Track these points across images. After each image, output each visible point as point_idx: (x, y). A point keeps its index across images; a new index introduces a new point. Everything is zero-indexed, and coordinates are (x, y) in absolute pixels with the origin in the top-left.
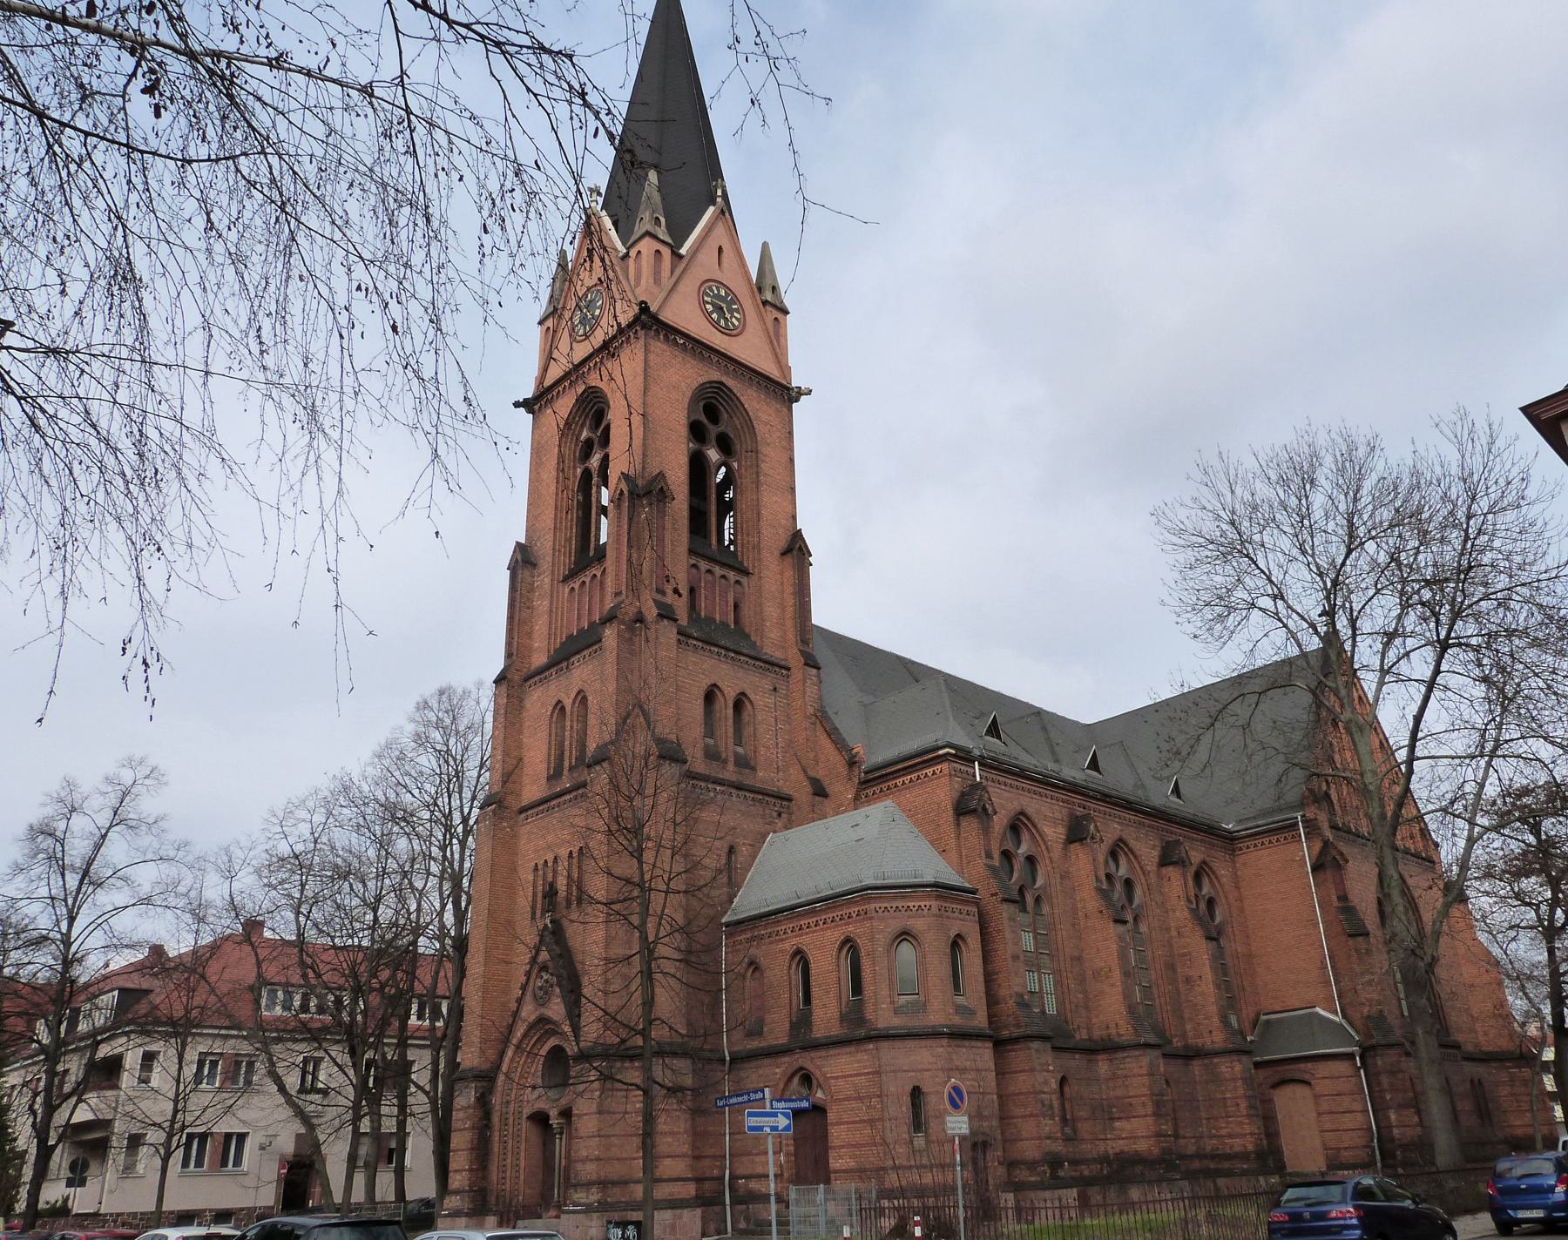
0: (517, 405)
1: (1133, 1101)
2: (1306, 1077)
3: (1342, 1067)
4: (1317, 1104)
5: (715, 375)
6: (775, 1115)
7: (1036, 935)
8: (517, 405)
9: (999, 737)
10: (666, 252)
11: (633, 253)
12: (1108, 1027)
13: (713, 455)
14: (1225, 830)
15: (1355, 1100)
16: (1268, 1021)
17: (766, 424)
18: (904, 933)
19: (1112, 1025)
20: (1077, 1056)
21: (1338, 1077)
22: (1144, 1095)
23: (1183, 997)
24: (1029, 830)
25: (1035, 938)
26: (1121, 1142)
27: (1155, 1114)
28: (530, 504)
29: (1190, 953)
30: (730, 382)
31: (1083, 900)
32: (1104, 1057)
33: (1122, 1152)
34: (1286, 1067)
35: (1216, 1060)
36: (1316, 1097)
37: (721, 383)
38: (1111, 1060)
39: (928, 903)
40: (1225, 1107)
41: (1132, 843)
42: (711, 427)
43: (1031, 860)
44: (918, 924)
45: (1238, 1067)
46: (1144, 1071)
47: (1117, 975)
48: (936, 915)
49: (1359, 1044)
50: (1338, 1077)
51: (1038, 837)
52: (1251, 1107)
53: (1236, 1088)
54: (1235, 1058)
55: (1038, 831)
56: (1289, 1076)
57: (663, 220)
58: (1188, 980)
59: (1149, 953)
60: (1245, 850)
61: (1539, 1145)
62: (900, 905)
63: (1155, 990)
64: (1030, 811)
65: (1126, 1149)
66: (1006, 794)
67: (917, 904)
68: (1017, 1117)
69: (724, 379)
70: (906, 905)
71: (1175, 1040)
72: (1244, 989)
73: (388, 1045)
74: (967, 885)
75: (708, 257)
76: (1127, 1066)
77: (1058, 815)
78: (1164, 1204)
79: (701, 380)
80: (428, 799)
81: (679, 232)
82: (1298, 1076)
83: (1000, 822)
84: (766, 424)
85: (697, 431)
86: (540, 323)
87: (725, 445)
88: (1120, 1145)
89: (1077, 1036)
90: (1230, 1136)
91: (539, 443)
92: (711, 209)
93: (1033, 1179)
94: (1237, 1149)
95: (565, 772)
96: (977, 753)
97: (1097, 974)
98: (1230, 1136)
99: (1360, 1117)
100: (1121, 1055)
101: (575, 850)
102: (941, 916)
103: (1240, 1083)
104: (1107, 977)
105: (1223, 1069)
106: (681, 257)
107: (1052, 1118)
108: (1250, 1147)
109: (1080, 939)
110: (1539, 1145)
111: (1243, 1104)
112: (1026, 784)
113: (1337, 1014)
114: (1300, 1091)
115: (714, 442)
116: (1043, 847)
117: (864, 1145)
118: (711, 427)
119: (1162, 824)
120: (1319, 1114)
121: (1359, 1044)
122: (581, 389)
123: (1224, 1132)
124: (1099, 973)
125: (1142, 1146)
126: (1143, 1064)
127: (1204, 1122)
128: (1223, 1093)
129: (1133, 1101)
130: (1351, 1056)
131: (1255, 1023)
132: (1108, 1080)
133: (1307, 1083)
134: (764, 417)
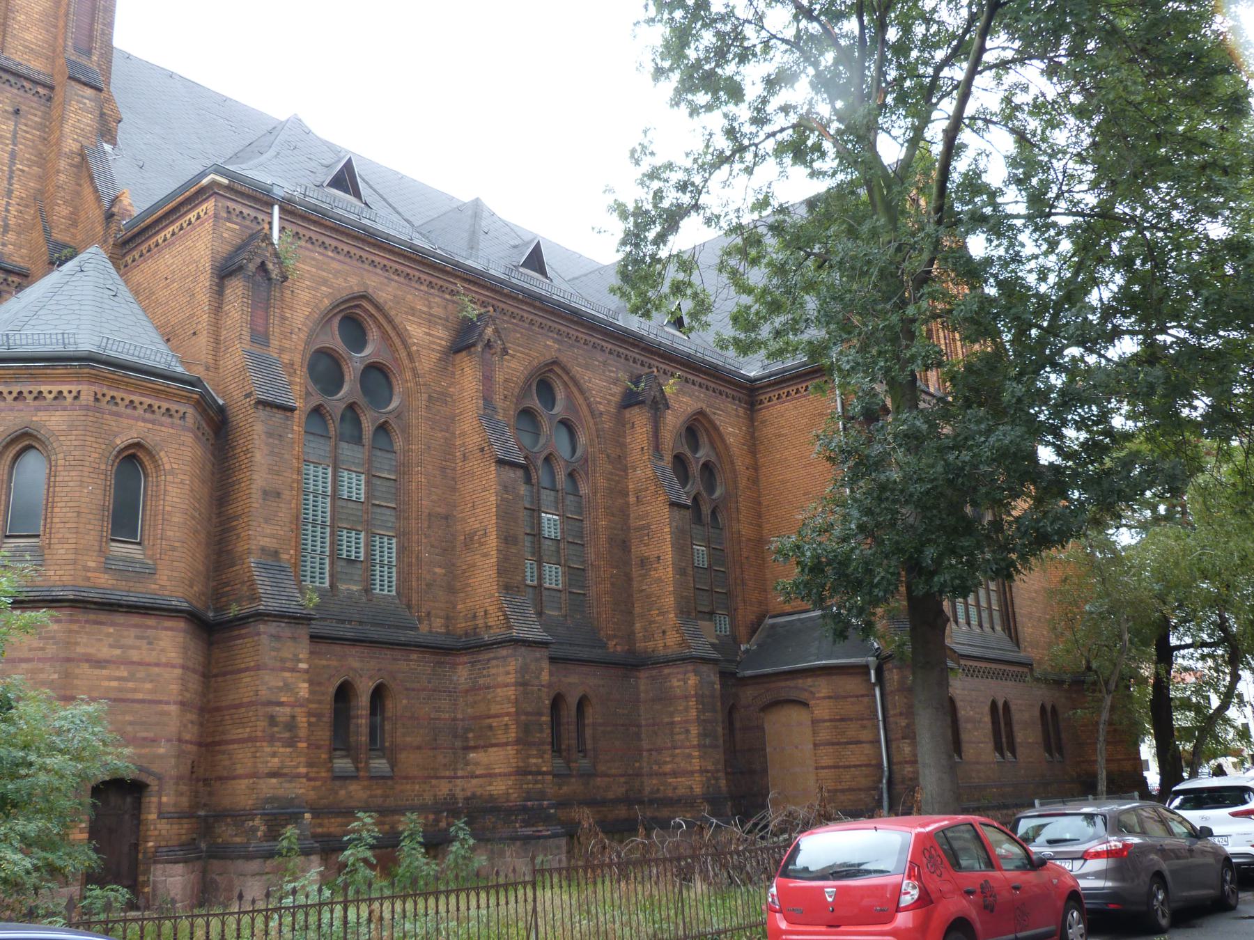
1: (494, 722)
2: (804, 696)
3: (851, 685)
4: (814, 733)
7: (371, 477)
9: (357, 194)
12: (475, 617)
14: (743, 377)
15: (864, 727)
16: (773, 626)
18: (25, 435)
19: (481, 613)
20: (414, 656)
21: (846, 697)
22: (508, 714)
23: (635, 585)
24: (380, 326)
25: (368, 483)
26: (474, 781)
27: (518, 742)
29: (647, 526)
31: (463, 434)
32: (465, 659)
33: (474, 796)
34: (783, 684)
35: (666, 671)
36: (814, 722)
38: (473, 663)
39: (75, 388)
40: (672, 734)
41: (577, 370)
43: (707, 467)
44: (52, 421)
45: (692, 680)
46: (511, 679)
47: (492, 540)
48: (87, 408)
50: (846, 697)
51: (394, 335)
52: (703, 735)
53: (687, 709)
54: (690, 668)
55: (394, 328)
56: (784, 695)
58: (643, 562)
59: (587, 524)
60: (767, 404)
61: (1102, 786)
62: (25, 389)
63: (590, 574)
64: (564, 359)
65: (479, 791)
66: (335, 265)
68: (233, 742)
70: (35, 388)
71: (611, 644)
72: (743, 583)
74: (180, 369)
76: (493, 671)
77: (437, 311)
78: (547, 875)
82: (794, 695)
83: (673, 421)
88: (473, 786)
89: (424, 628)
90: (675, 774)
93: (238, 840)
94: (681, 791)
96: (278, 192)
97: (470, 538)
98: (675, 774)
99: (867, 749)
100: (485, 656)
102: (96, 410)
103: (692, 703)
104: (481, 544)
105: (675, 683)
107: (291, 743)
108: (698, 790)
109: (454, 490)
110: (1102, 786)
111: (694, 731)
112: (380, 257)
114: (795, 716)
116: (403, 354)
119: (634, 353)
120: (816, 745)
123: (668, 768)
124: (472, 540)
125: (498, 787)
126: (511, 668)
127: (645, 754)
128: (671, 714)
129: (494, 722)
130: (865, 669)
131: (753, 630)
132: (467, 691)
133: (805, 704)
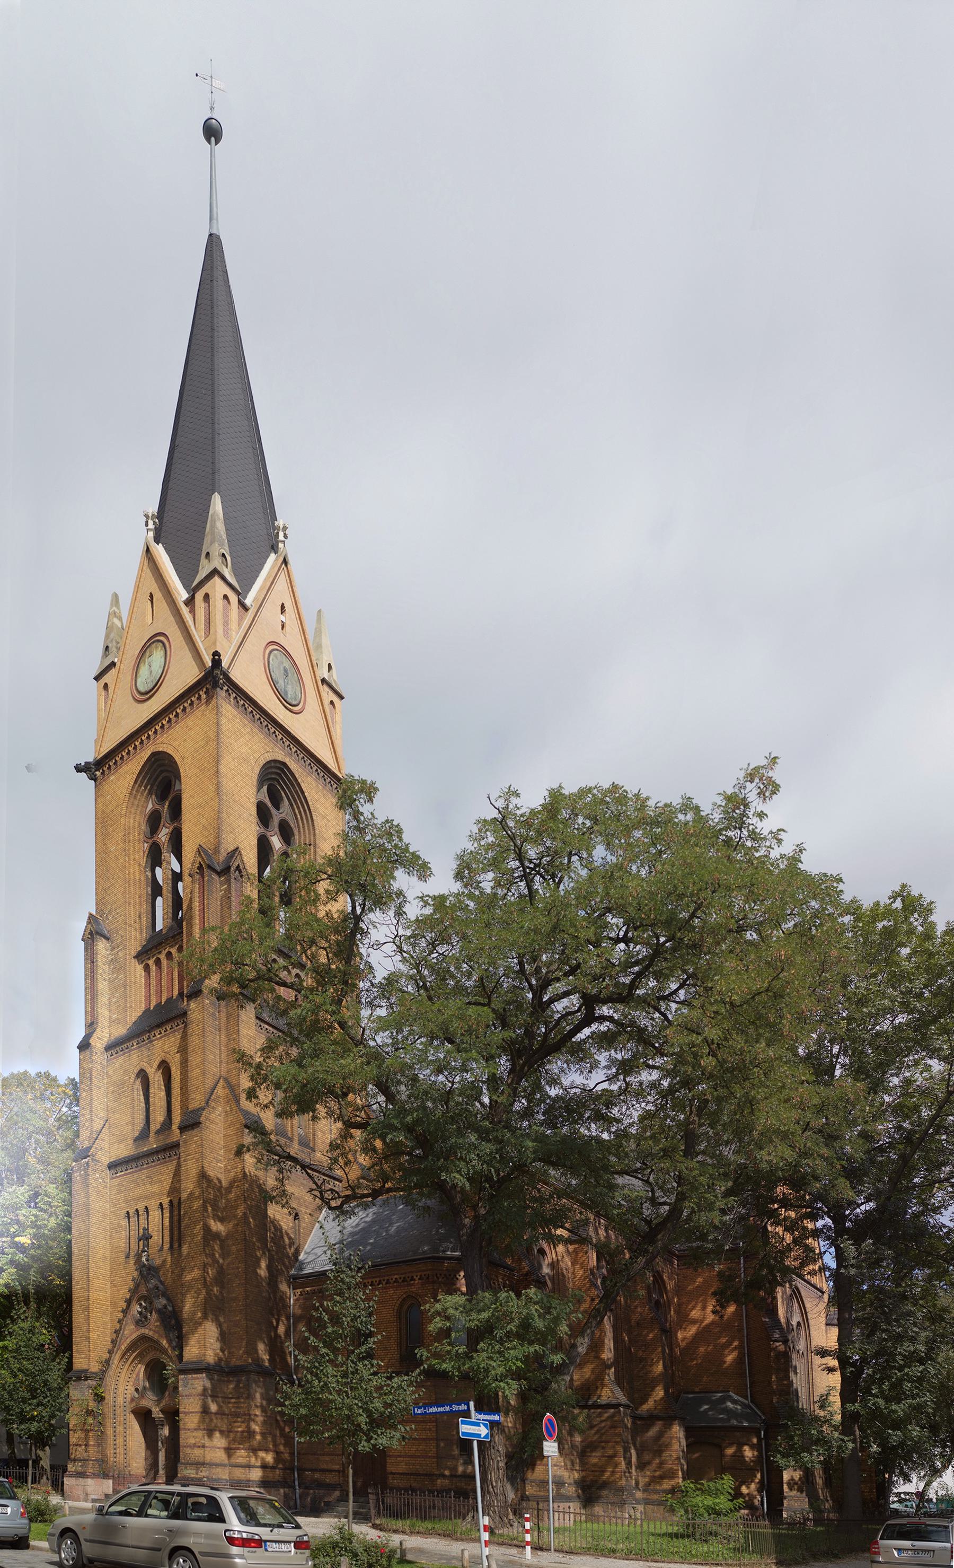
0: (79, 769)
5: (280, 755)
6: (478, 1425)
8: (79, 769)
10: (233, 598)
11: (199, 596)
13: (276, 842)
17: (324, 817)
28: (98, 876)
30: (293, 765)
37: (284, 764)
42: (274, 811)
49: (764, 1421)
57: (229, 558)
67: (403, 1276)
69: (287, 761)
73: (816, 1233)
75: (271, 613)
78: (567, 1516)
79: (269, 757)
80: (681, 888)
81: (247, 575)
84: (324, 817)
85: (263, 815)
86: (97, 678)
87: (286, 833)
91: (103, 812)
92: (273, 556)
95: (152, 1134)
101: (132, 1212)
106: (246, 609)
113: (746, 1398)
115: (277, 829)
117: (419, 1457)
118: (274, 811)
121: (764, 1421)
122: (145, 755)
134: (321, 810)
